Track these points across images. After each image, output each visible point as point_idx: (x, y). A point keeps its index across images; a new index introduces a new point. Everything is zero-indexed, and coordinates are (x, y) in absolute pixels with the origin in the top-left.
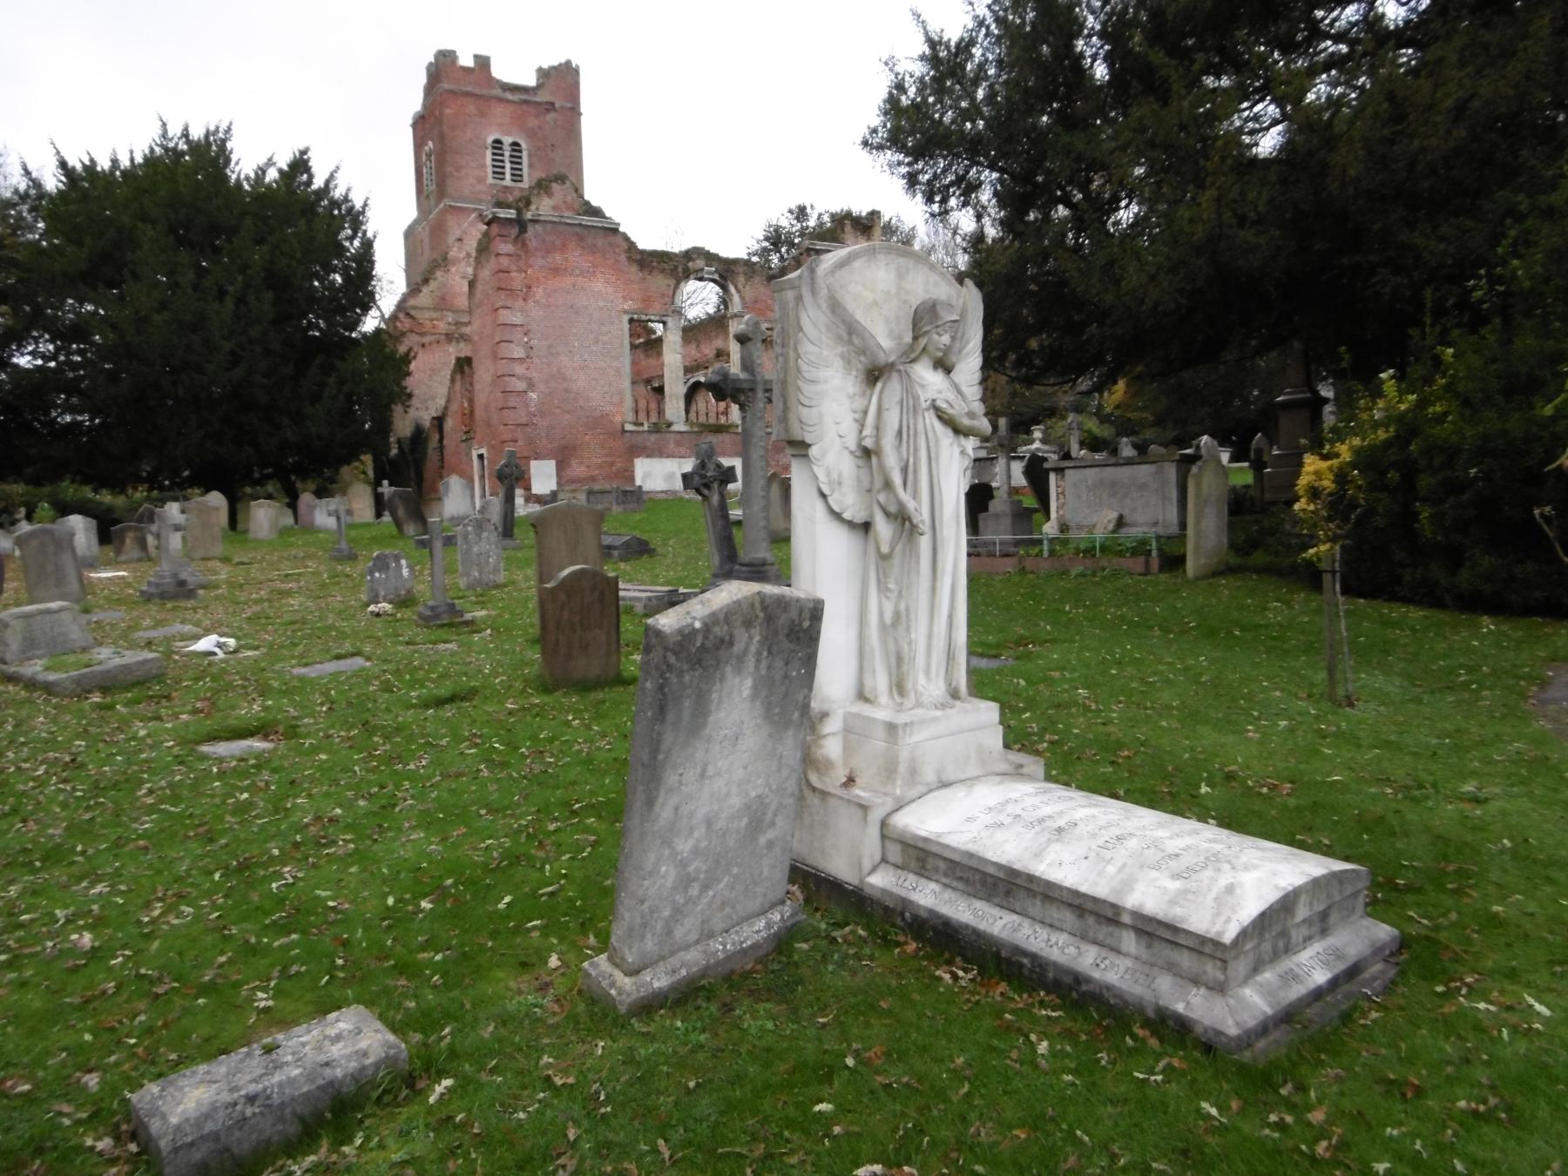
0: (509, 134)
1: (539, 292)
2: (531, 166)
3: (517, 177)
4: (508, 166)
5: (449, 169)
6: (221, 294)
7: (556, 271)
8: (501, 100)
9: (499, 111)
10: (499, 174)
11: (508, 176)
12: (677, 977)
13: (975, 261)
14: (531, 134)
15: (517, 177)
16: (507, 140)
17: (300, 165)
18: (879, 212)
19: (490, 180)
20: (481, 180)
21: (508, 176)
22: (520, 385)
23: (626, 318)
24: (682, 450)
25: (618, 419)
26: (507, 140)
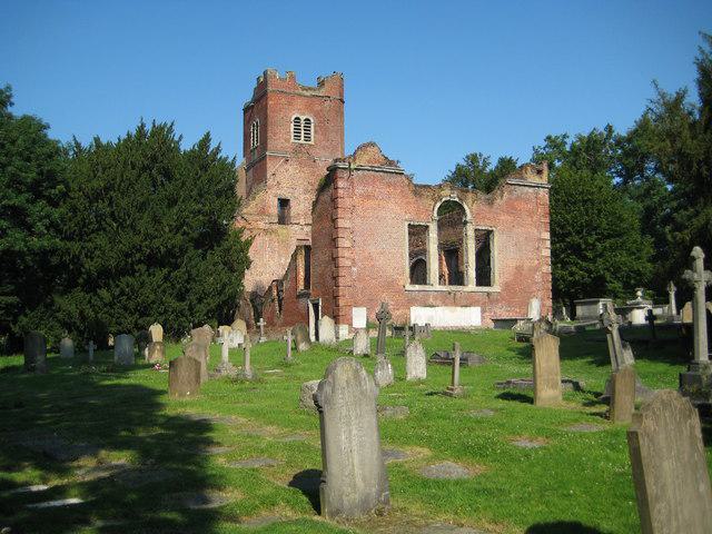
0: (303, 114)
1: (359, 210)
2: (315, 132)
3: (308, 138)
4: (303, 132)
5: (269, 134)
6: (172, 202)
7: (368, 197)
8: (300, 95)
9: (299, 102)
10: (297, 137)
11: (302, 138)
12: (315, 467)
13: (57, 151)
14: (316, 115)
15: (308, 138)
16: (303, 118)
17: (97, 140)
18: (510, 161)
19: (292, 140)
20: (287, 140)
21: (302, 138)
22: (348, 263)
23: (407, 224)
24: (438, 302)
25: (401, 283)
26: (303, 118)
